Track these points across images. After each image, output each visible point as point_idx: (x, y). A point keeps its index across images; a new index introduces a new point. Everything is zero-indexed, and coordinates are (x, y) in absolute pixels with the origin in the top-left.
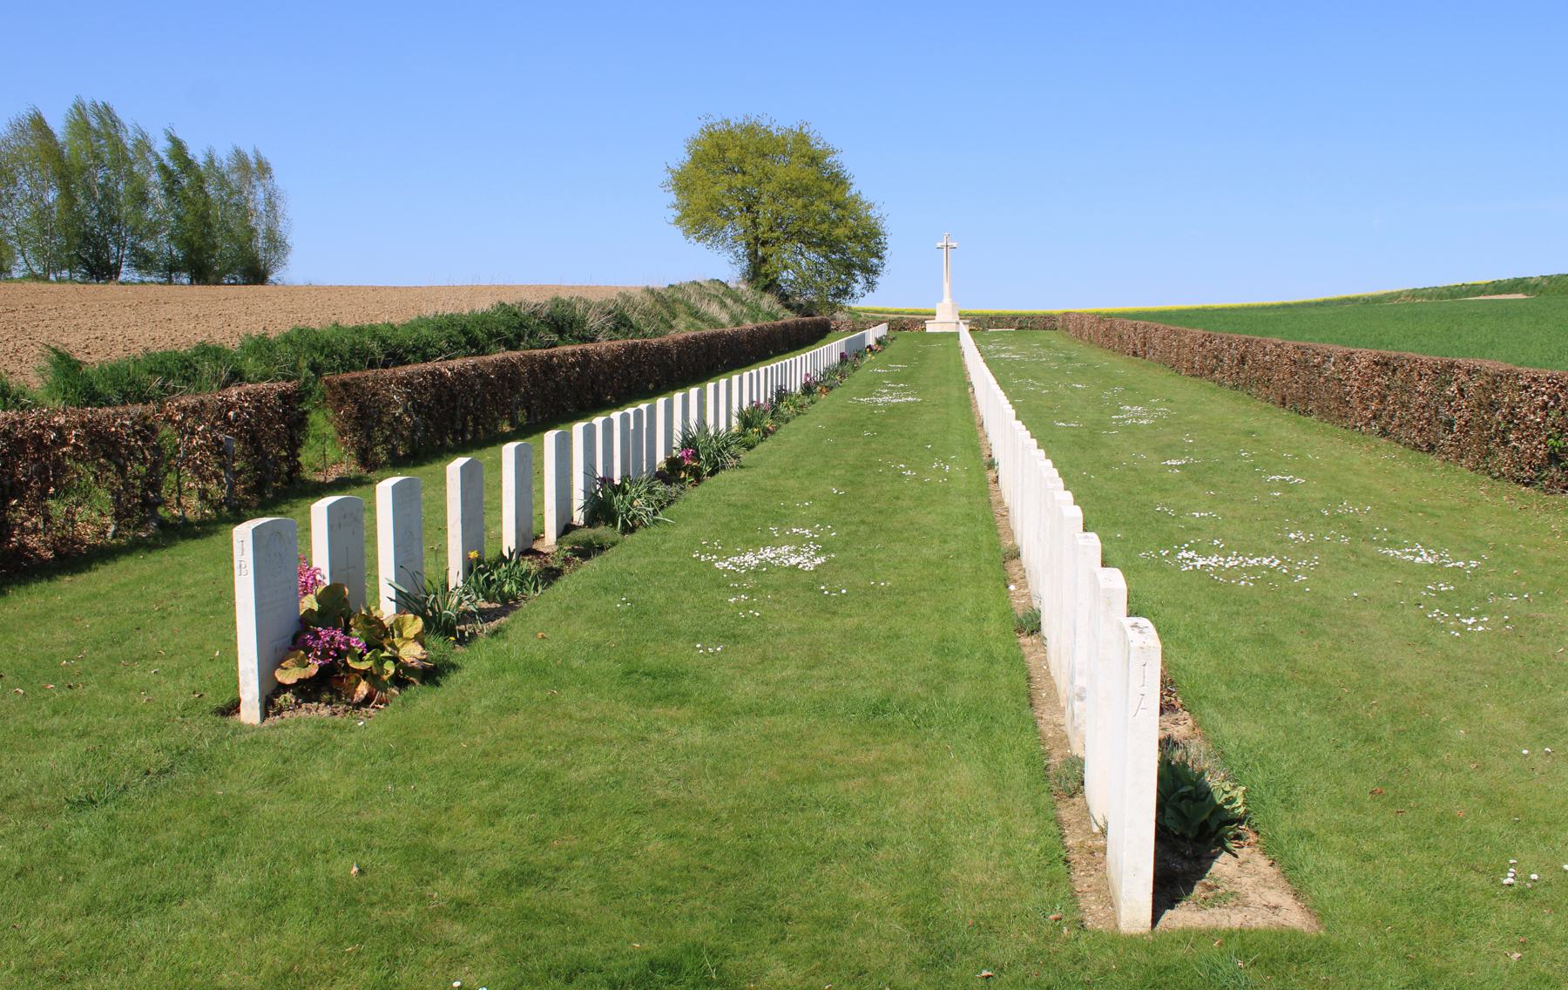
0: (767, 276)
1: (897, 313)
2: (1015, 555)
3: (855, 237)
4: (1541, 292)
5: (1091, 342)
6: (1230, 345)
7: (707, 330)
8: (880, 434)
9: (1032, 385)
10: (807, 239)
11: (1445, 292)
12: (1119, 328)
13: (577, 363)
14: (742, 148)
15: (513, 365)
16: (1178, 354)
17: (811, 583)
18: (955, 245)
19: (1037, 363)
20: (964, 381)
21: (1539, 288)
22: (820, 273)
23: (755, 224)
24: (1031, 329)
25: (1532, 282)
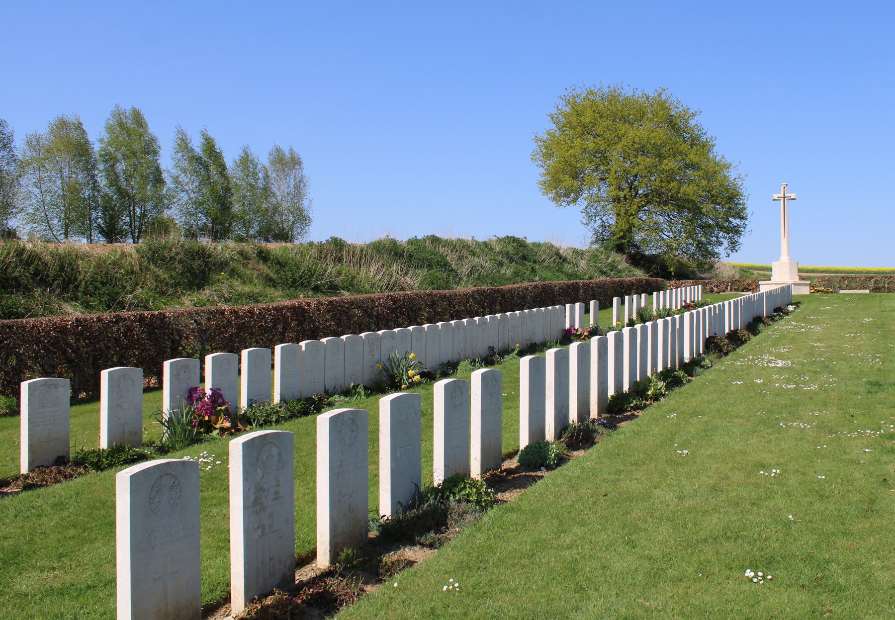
18: (793, 196)
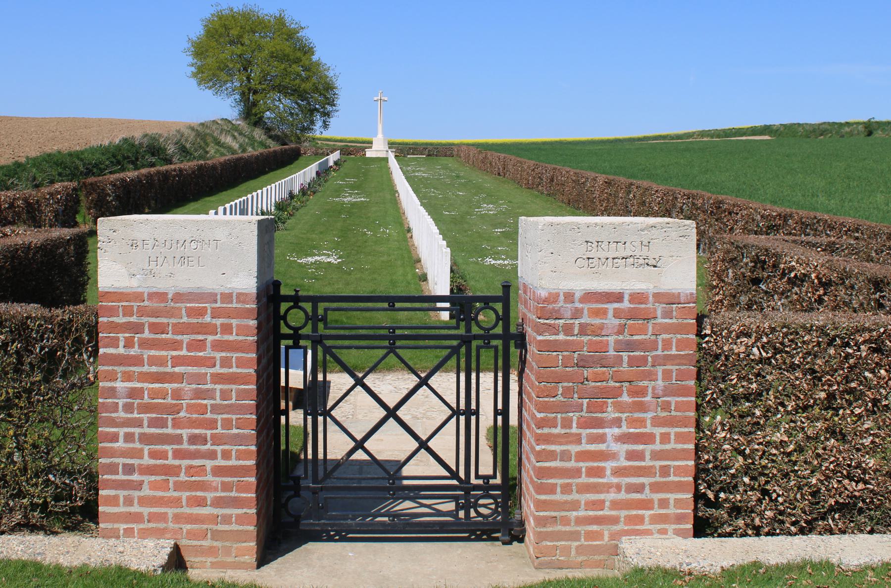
0: (256, 115)
1: (341, 141)
2: (419, 261)
3: (316, 89)
4: (779, 135)
5: (474, 166)
6: (546, 171)
7: (229, 157)
8: (350, 216)
9: (434, 192)
10: (282, 89)
11: (722, 133)
12: (490, 158)
13: (177, 175)
14: (241, 28)
15: (151, 175)
16: (521, 176)
17: (339, 267)
18: (386, 99)
19: (438, 179)
20: (393, 190)
21: (778, 132)
22: (292, 114)
23: (248, 79)
24: (436, 156)
25: (775, 127)
